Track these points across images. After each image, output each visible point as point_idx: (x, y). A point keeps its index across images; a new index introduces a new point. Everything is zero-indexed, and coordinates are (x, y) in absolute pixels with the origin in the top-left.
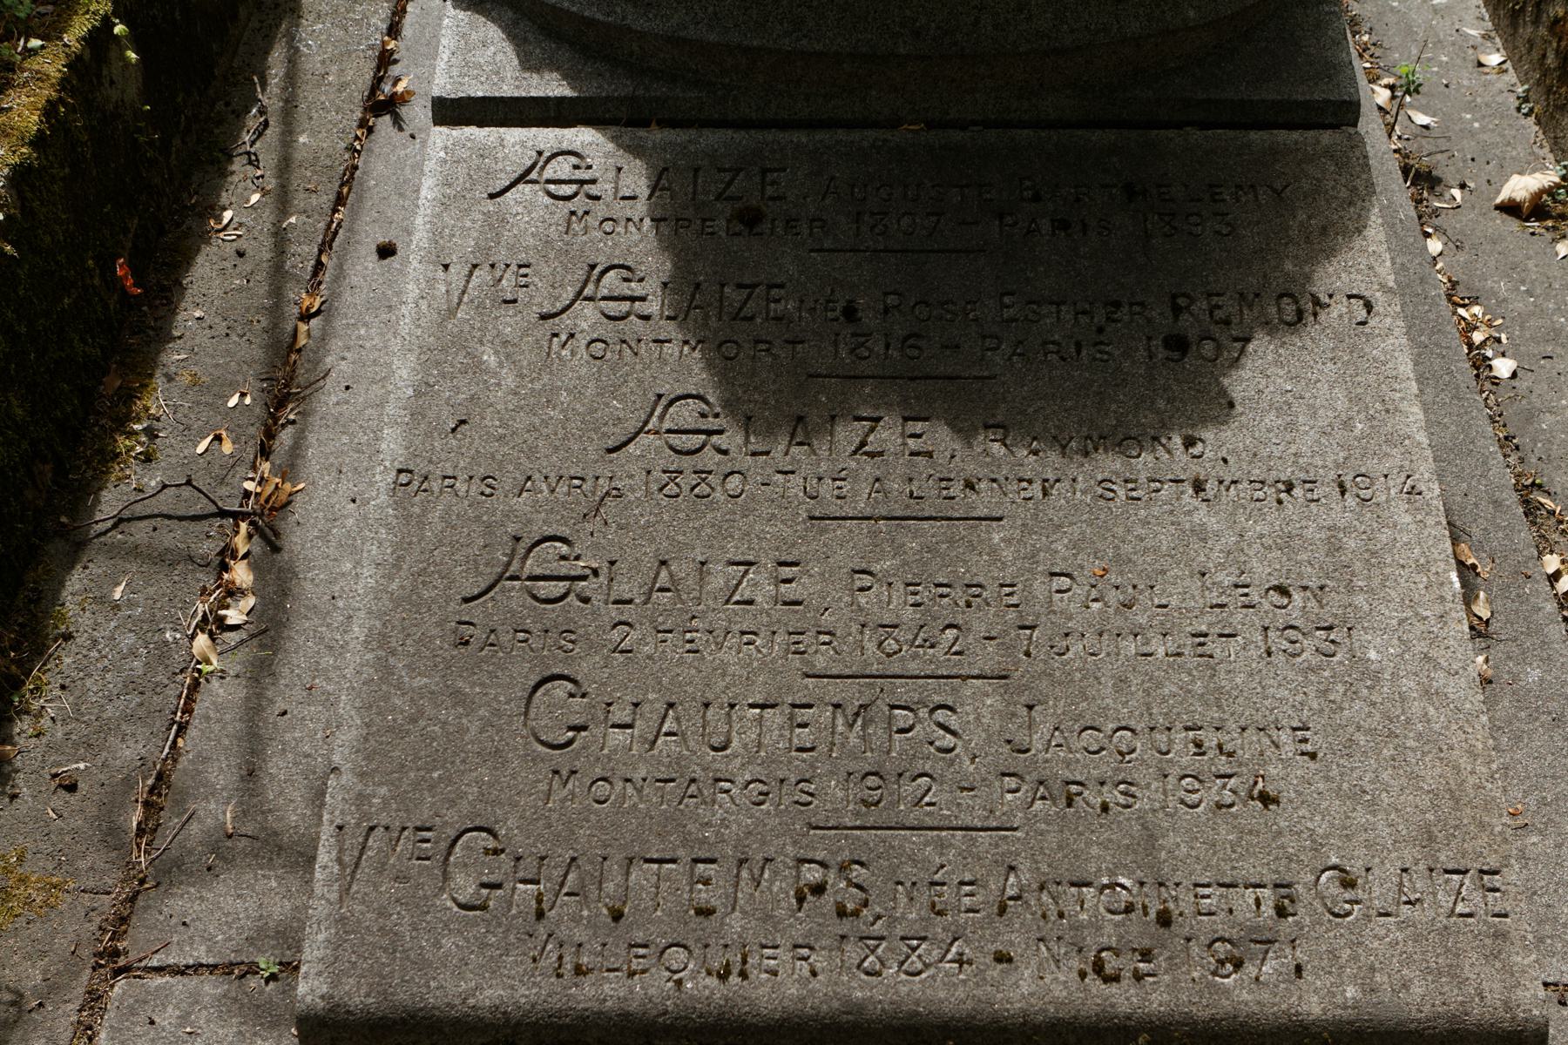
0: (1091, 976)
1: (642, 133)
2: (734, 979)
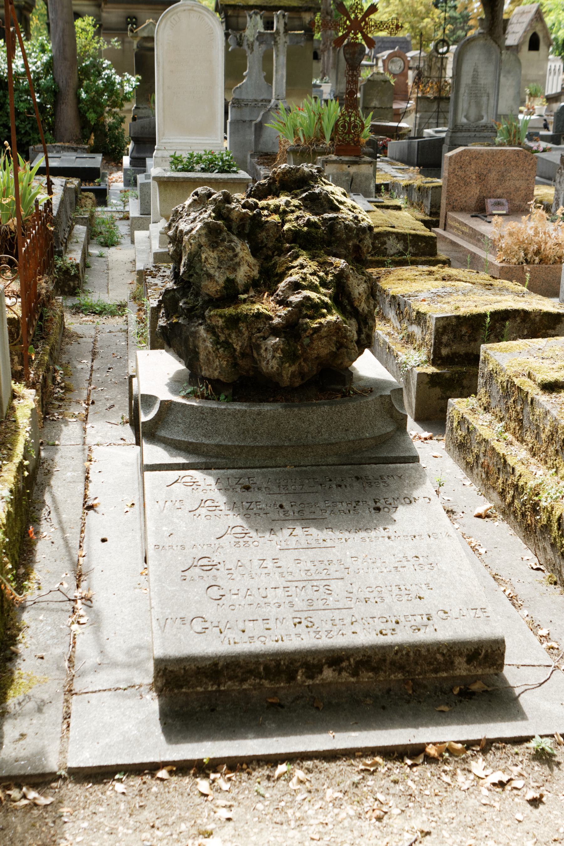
0: (379, 635)
1: (210, 471)
2: (280, 642)
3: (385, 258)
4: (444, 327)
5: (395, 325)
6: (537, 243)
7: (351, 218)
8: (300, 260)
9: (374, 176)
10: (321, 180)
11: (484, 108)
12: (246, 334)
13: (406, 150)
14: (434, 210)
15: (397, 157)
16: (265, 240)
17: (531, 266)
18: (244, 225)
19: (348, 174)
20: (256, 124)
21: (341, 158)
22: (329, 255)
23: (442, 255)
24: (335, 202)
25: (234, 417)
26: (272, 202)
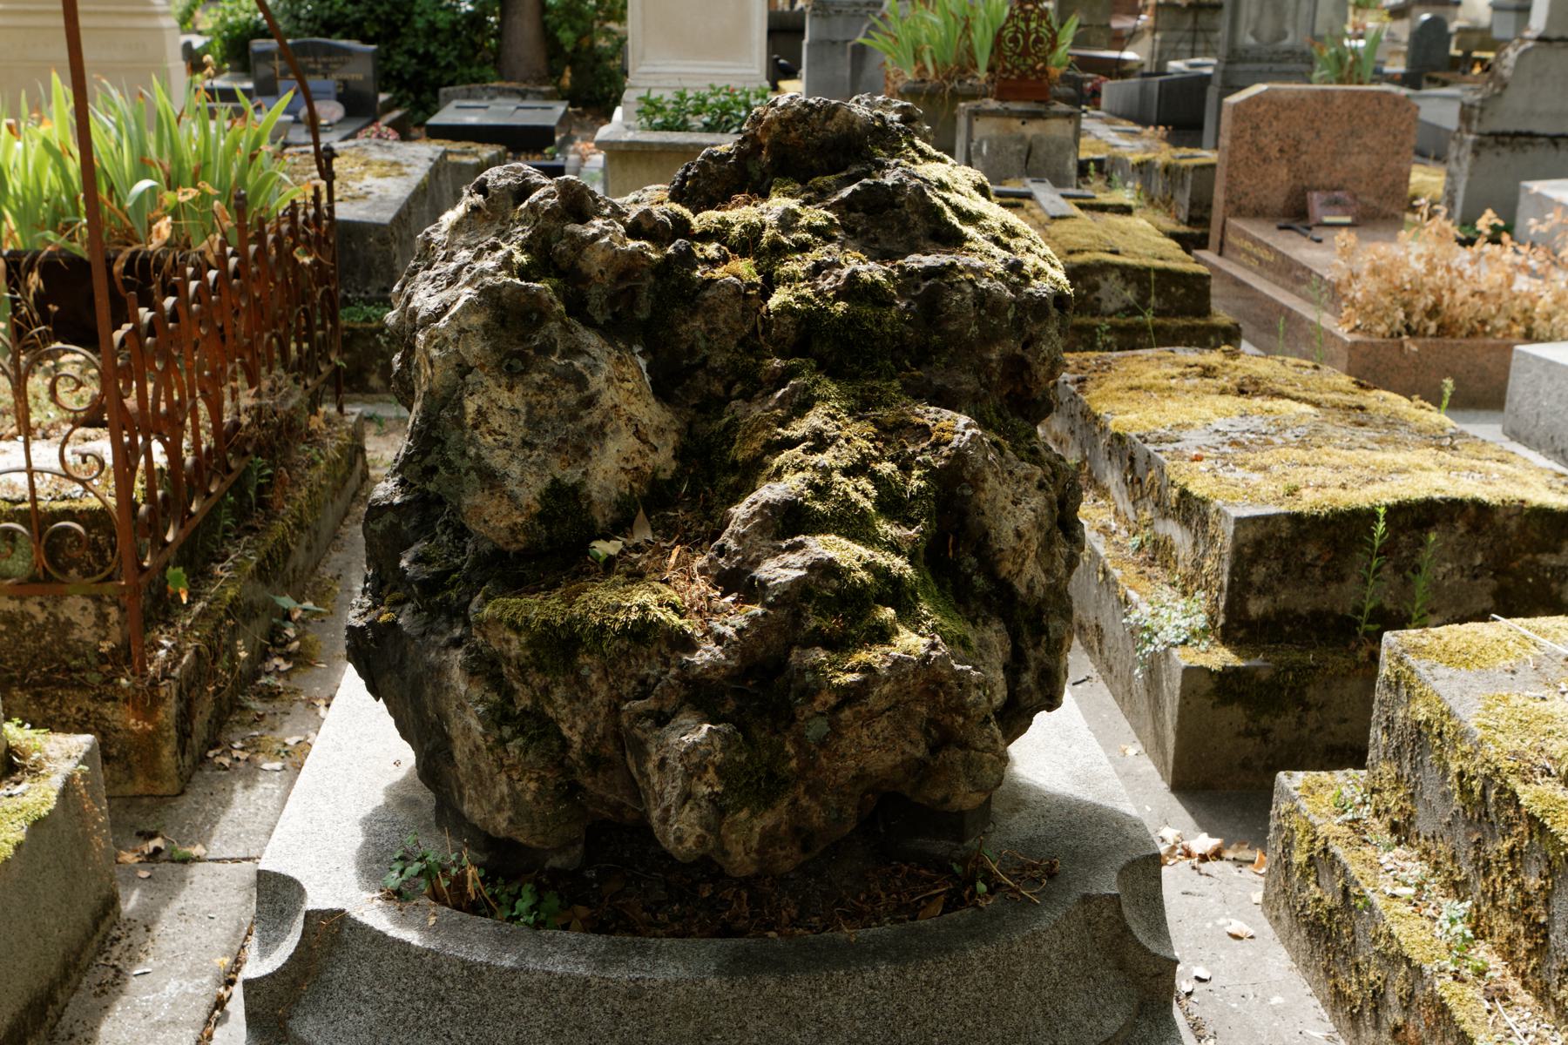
3: (1096, 321)
4: (1259, 544)
5: (1121, 507)
6: (1432, 291)
7: (999, 269)
8: (815, 419)
9: (1077, 143)
10: (914, 146)
11: (1289, 16)
12: (603, 692)
13: (1137, 98)
14: (1197, 213)
15: (1119, 111)
16: (702, 344)
17: (1420, 341)
18: (632, 293)
19: (1022, 139)
20: (854, 47)
21: (1007, 105)
22: (918, 398)
23: (1222, 316)
24: (949, 213)
25: (546, 1000)
26: (740, 214)
